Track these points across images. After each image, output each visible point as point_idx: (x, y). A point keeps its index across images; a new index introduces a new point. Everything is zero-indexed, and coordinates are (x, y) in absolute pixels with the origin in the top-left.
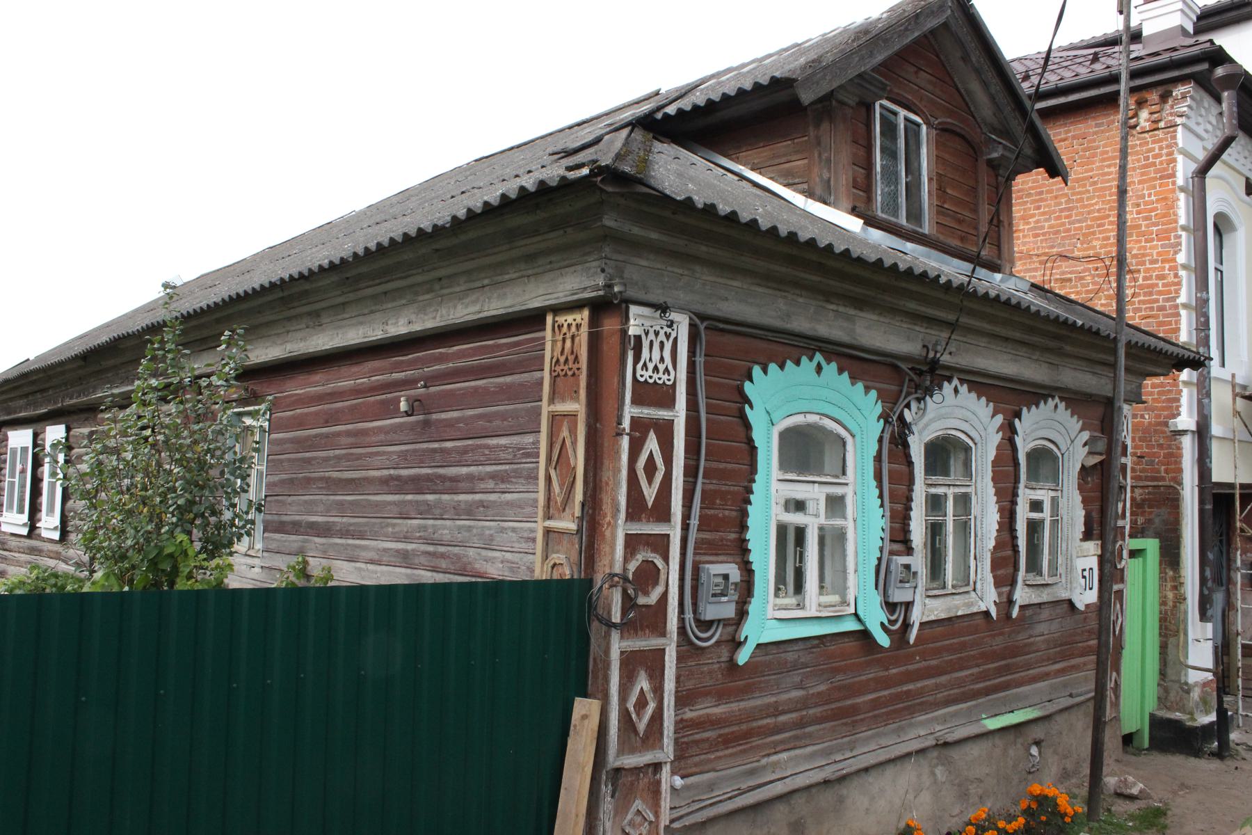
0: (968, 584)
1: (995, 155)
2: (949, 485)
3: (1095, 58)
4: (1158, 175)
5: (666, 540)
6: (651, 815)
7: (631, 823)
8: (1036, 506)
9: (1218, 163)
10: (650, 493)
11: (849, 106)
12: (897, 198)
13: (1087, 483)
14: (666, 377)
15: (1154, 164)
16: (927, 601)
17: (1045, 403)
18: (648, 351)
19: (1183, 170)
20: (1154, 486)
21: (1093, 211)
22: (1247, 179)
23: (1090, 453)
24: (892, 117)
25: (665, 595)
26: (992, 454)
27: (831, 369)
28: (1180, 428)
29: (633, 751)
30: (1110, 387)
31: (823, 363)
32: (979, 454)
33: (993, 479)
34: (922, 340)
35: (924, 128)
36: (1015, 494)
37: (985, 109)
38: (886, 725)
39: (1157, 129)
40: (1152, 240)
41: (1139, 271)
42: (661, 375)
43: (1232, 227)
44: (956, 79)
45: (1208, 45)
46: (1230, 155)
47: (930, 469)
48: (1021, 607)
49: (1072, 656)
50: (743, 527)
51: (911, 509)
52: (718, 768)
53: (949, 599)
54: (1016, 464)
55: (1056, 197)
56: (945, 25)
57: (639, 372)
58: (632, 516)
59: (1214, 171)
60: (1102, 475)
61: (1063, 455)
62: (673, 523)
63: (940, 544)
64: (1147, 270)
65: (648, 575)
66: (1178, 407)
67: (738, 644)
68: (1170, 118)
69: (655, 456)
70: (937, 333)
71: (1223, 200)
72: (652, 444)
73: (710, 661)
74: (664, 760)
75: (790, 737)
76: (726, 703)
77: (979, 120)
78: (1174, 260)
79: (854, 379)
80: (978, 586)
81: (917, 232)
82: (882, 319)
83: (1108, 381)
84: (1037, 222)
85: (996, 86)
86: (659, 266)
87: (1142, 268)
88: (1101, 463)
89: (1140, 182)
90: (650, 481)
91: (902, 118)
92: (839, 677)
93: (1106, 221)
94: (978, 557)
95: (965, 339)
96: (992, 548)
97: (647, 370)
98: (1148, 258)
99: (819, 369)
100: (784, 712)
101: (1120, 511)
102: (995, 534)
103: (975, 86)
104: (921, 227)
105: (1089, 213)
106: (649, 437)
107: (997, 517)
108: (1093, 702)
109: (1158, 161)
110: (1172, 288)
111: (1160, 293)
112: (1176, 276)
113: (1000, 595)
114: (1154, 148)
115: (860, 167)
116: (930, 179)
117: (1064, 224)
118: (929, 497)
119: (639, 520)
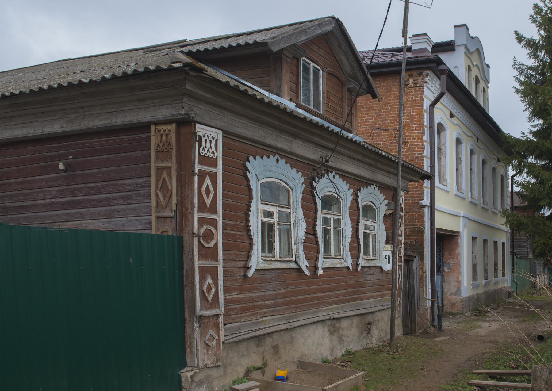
0: (340, 255)
1: (350, 86)
2: (332, 214)
3: (393, 56)
4: (416, 105)
5: (216, 221)
6: (216, 337)
7: (209, 340)
8: (367, 227)
9: (439, 103)
10: (208, 201)
11: (289, 58)
12: (309, 98)
13: (387, 221)
14: (213, 155)
15: (415, 100)
16: (324, 260)
17: (370, 187)
18: (205, 143)
19: (426, 104)
20: (413, 228)
21: (390, 117)
22: (450, 111)
23: (388, 209)
24: (307, 65)
25: (217, 243)
26: (349, 204)
27: (282, 161)
28: (423, 205)
29: (206, 309)
30: (396, 183)
31: (279, 159)
32: (344, 204)
33: (349, 214)
34: (320, 155)
35: (321, 72)
36: (358, 222)
37: (347, 68)
38: (309, 310)
39: (417, 87)
40: (413, 130)
41: (408, 142)
42: (210, 153)
43: (444, 130)
44: (335, 54)
45: (436, 57)
46: (444, 98)
47: (323, 208)
48: (361, 267)
49: (381, 291)
50: (247, 221)
51: (317, 222)
52: (242, 321)
53: (333, 260)
54: (358, 210)
55: (375, 110)
56: (331, 32)
57: (201, 151)
58: (200, 210)
59: (438, 105)
60: (393, 219)
61: (377, 209)
62: (218, 215)
63: (328, 238)
64: (411, 142)
65: (209, 236)
66: (423, 196)
67: (248, 268)
68: (421, 83)
69: (209, 186)
70: (326, 153)
71: (441, 118)
72: (208, 181)
73: (236, 275)
74: (220, 313)
75: (271, 311)
76: (244, 294)
77: (344, 72)
78: (422, 139)
79: (292, 167)
80: (344, 256)
81: (317, 113)
82: (304, 144)
83: (395, 181)
84: (367, 119)
85: (352, 59)
86: (208, 109)
87: (409, 141)
88: (392, 213)
89: (409, 107)
90: (208, 196)
91: (312, 66)
92: (290, 287)
93: (396, 121)
94: (344, 245)
95: (338, 157)
96: (349, 241)
97: (204, 151)
98: (411, 137)
99: (277, 161)
100: (267, 300)
101: (400, 233)
102: (351, 236)
103: (343, 58)
104: (319, 111)
105: (389, 117)
106: (207, 179)
107: (351, 229)
108: (390, 309)
109: (416, 99)
110: (421, 150)
111: (416, 151)
112: (423, 145)
113: (353, 261)
114: (415, 94)
115: (293, 83)
116: (323, 93)
117: (378, 121)
118: (323, 218)
119: (204, 212)
